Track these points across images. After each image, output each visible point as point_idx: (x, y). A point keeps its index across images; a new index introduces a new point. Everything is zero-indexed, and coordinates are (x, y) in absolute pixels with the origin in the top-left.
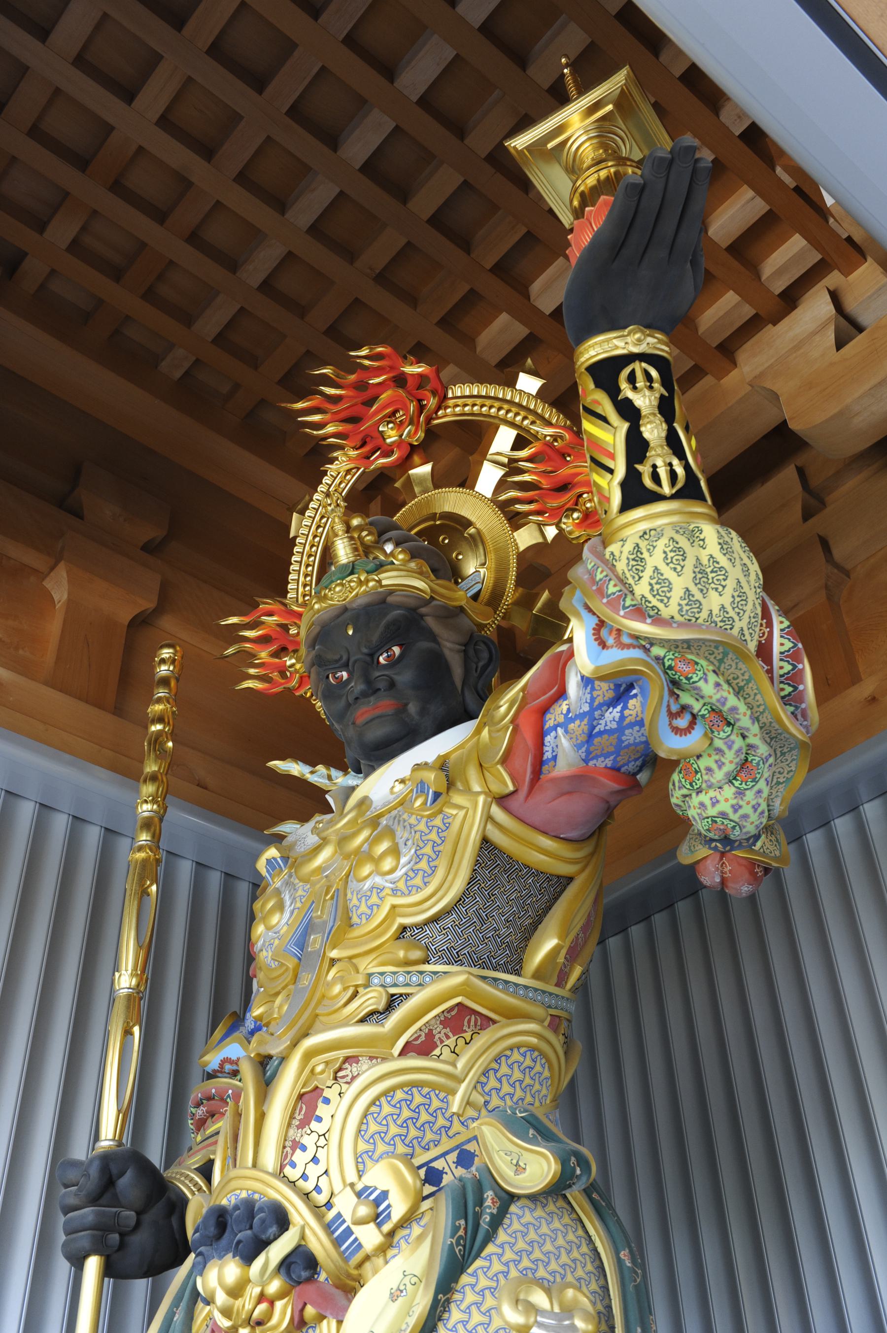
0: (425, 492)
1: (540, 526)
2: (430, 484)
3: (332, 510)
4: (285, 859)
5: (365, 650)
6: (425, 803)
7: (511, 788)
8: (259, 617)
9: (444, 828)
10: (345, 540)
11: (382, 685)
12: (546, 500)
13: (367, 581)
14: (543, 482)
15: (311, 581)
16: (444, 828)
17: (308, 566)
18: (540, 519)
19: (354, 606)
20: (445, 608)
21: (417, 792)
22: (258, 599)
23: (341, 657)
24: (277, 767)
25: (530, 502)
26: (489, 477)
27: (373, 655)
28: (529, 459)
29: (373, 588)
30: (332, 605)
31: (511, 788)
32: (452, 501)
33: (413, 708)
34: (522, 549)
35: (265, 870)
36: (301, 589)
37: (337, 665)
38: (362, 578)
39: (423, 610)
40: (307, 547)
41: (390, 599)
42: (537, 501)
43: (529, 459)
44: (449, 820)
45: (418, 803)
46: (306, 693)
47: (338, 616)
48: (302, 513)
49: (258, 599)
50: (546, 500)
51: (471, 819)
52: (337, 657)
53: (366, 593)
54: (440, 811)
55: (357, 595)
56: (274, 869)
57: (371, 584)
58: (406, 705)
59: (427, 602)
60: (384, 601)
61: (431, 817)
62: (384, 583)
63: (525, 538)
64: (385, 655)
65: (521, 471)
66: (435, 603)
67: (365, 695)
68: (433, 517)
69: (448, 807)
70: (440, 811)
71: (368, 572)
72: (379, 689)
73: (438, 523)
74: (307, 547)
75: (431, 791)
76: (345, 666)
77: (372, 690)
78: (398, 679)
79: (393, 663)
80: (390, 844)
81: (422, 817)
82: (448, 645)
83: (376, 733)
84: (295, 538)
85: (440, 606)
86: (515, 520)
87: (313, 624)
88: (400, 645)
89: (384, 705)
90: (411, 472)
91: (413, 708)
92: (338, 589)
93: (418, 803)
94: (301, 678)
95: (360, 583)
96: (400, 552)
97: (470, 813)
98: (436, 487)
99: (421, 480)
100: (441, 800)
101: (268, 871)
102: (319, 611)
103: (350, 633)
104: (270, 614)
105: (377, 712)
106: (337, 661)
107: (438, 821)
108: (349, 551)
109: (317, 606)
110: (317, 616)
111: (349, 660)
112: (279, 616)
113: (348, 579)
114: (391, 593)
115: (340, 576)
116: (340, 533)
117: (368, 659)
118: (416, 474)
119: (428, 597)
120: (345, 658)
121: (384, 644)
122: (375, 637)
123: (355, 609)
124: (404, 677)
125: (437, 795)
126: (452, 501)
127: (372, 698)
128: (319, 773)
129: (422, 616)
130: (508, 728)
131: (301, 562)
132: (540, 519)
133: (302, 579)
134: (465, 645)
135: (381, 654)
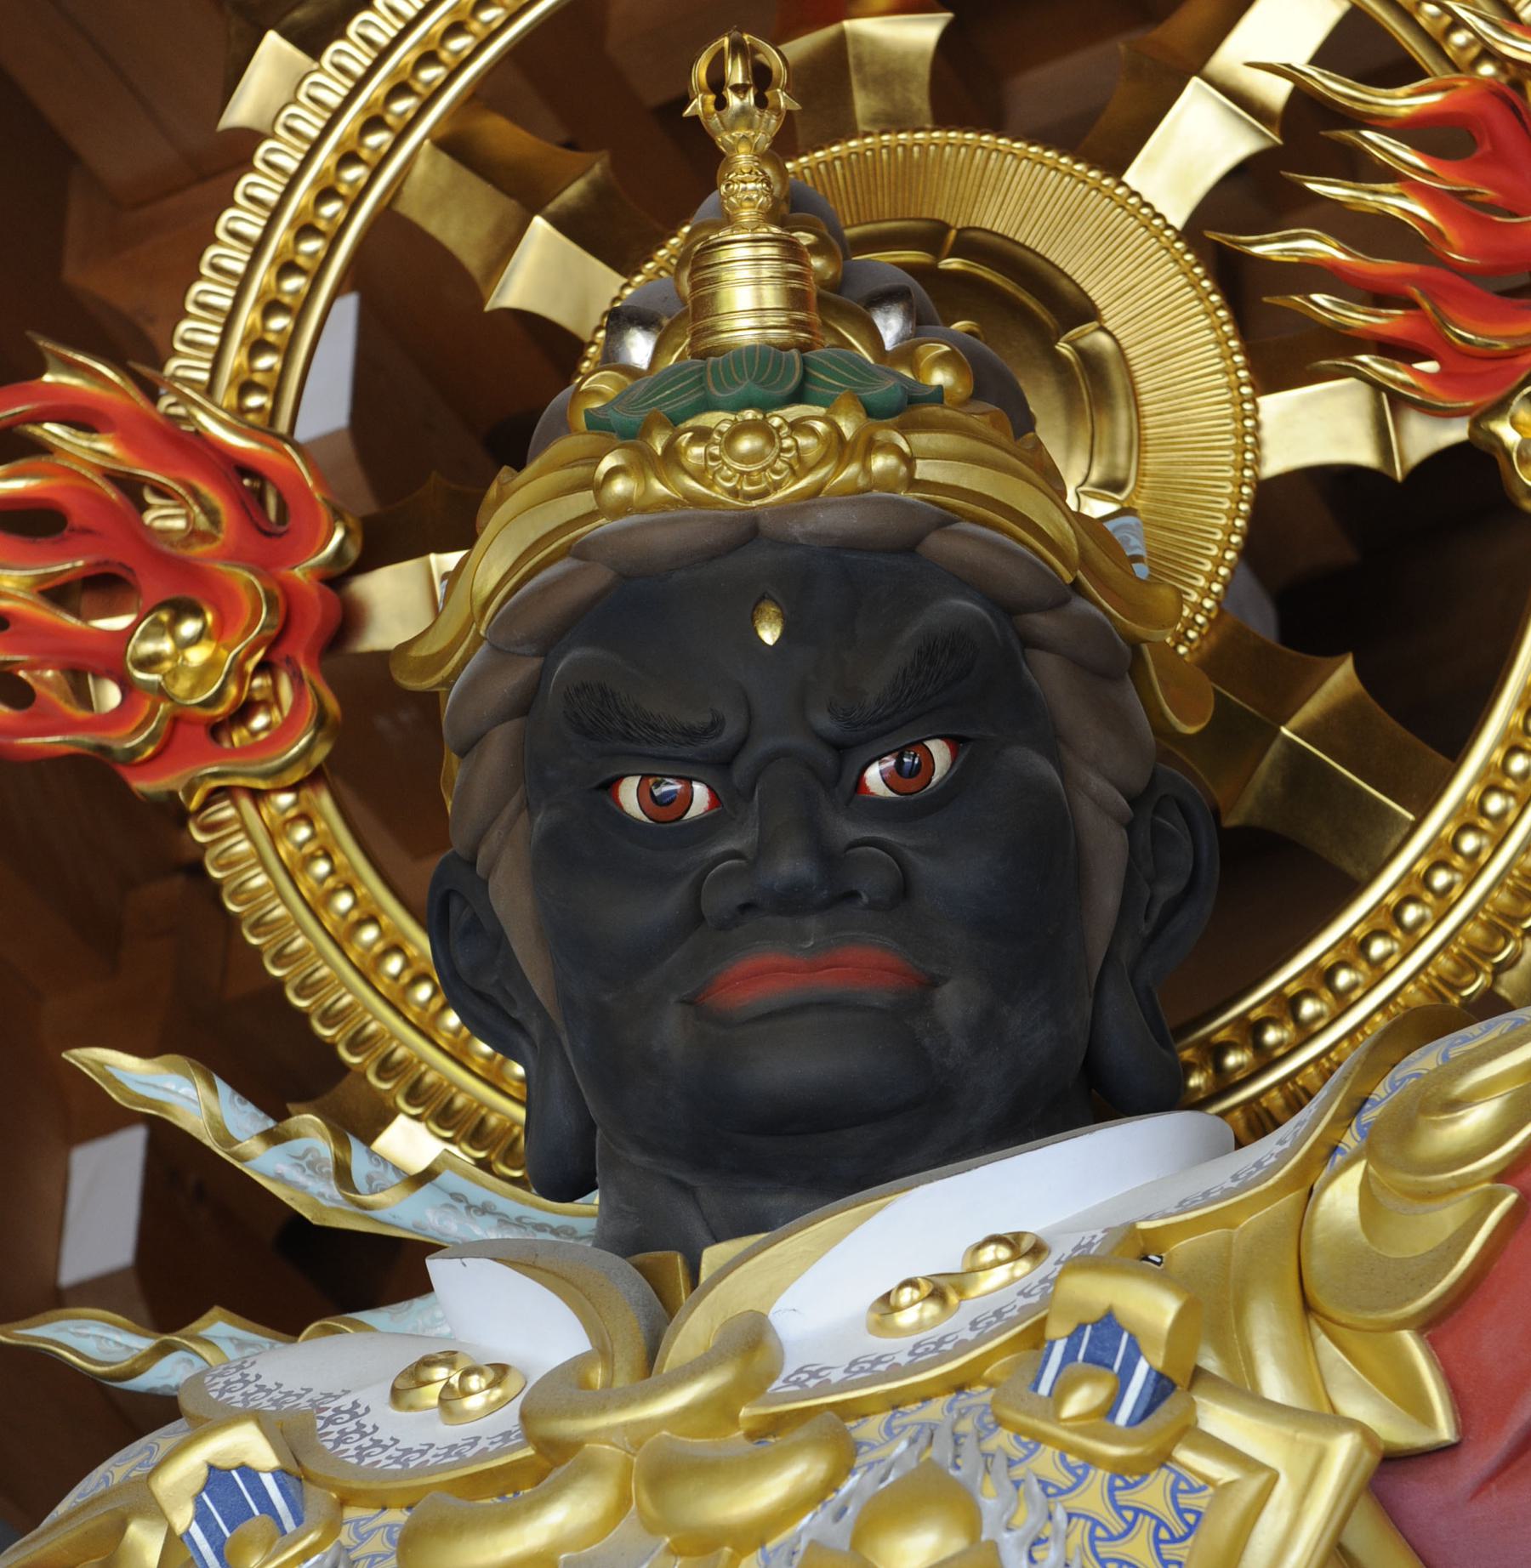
0: (895, 121)
1: (1391, 404)
2: (920, 99)
3: (744, 111)
4: (293, 1476)
5: (824, 721)
6: (1110, 1409)
7: (1445, 1430)
8: (38, 419)
9: (1180, 1530)
10: (767, 250)
11: (871, 883)
12: (1449, 311)
13: (871, 447)
14: (1451, 234)
15: (294, 336)
16: (1180, 1530)
17: (288, 268)
18: (1402, 376)
19: (796, 529)
20: (1099, 630)
21: (1069, 1356)
22: (44, 344)
23: (716, 725)
24: (110, 1079)
25: (1378, 297)
26: (1194, 146)
27: (847, 753)
28: (1409, 130)
29: (884, 481)
30: (693, 500)
31: (1445, 1430)
32: (1018, 191)
33: (955, 1002)
34: (1274, 465)
35: (189, 1510)
36: (235, 358)
37: (686, 751)
38: (847, 428)
39: (1042, 624)
40: (302, 195)
41: (936, 543)
42: (1409, 304)
43: (1409, 130)
44: (1200, 1502)
45: (1080, 1401)
46: (190, 790)
47: (713, 554)
48: (312, 41)
49: (44, 344)
50: (1449, 311)
51: (1284, 1517)
52: (698, 719)
53: (854, 495)
54: (1163, 1459)
55: (816, 491)
56: (237, 1515)
57: (879, 463)
58: (934, 983)
59: (1065, 595)
60: (909, 547)
61: (1126, 1473)
62: (925, 470)
63: (1318, 427)
64: (890, 762)
65: (1359, 167)
66: (1080, 605)
67: (792, 902)
68: (932, 237)
69: (1194, 1447)
70: (1163, 1459)
71: (872, 412)
72: (853, 895)
73: (953, 264)
74: (302, 195)
75: (1142, 1369)
76: (718, 767)
77: (830, 893)
78: (926, 868)
79: (916, 804)
80: (957, 1544)
81: (1092, 1460)
82: (1097, 783)
83: (790, 1067)
84: (250, 138)
85: (1097, 620)
86: (1280, 350)
87: (578, 550)
88: (955, 742)
89: (857, 962)
90: (847, 24)
91: (955, 1002)
92: (746, 444)
93: (1080, 1401)
94: (177, 720)
95: (839, 449)
96: (942, 360)
97: (1283, 1492)
98: (947, 114)
99: (889, 71)
100: (1167, 1411)
101: (202, 1516)
102: (625, 506)
103: (769, 634)
104: (84, 419)
105: (826, 984)
106: (692, 735)
107: (1153, 1493)
108: (771, 296)
109: (619, 486)
110: (604, 524)
111: (742, 744)
112: (127, 439)
113: (794, 412)
114: (945, 520)
115: (757, 392)
116: (746, 215)
117: (827, 759)
118: (873, 42)
119: (1069, 579)
120: (732, 730)
121: (892, 727)
122: (876, 684)
123: (794, 544)
124: (957, 873)
125: (1161, 1388)
126: (1018, 191)
127: (812, 924)
128: (297, 1146)
129: (1030, 642)
130: (1491, 1201)
131: (259, 247)
132: (1402, 376)
133: (248, 316)
134: (1132, 802)
135: (879, 758)
